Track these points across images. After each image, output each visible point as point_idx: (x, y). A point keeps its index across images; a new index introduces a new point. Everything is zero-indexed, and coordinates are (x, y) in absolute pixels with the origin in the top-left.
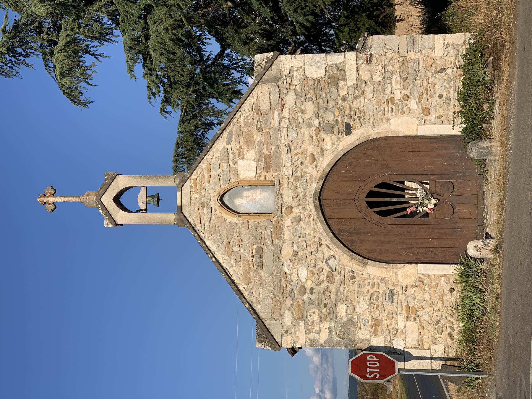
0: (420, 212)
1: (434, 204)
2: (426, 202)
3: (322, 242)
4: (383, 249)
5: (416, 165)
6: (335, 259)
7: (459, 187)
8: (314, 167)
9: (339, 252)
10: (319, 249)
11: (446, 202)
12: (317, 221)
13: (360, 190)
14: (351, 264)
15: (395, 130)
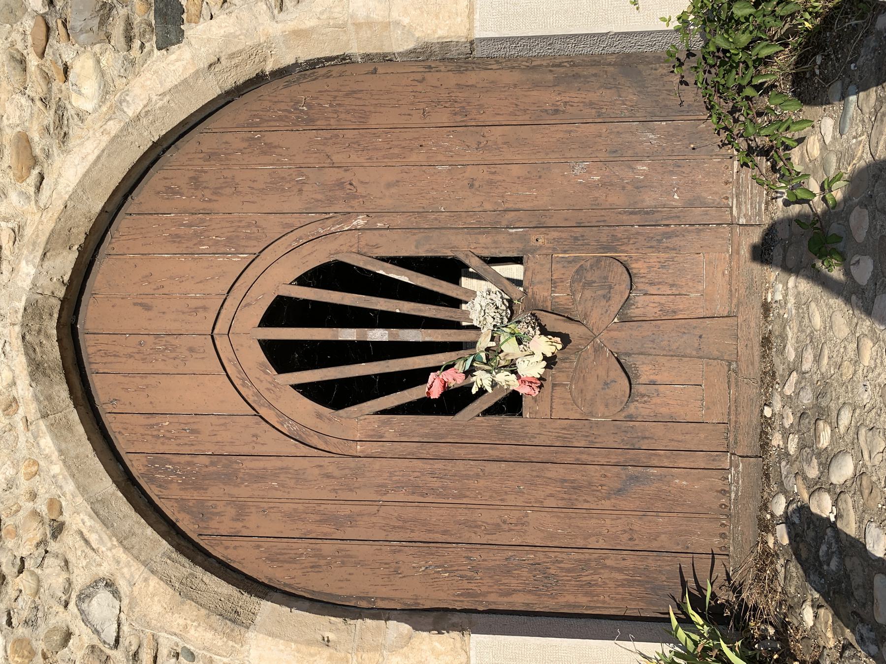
0: (482, 391)
1: (545, 358)
2: (510, 347)
3: (66, 517)
4: (328, 548)
5: (471, 186)
6: (116, 593)
7: (651, 284)
8: (32, 190)
9: (128, 565)
10: (53, 546)
11: (598, 350)
12: (38, 426)
13: (238, 293)
14: (177, 621)
15: (374, 16)
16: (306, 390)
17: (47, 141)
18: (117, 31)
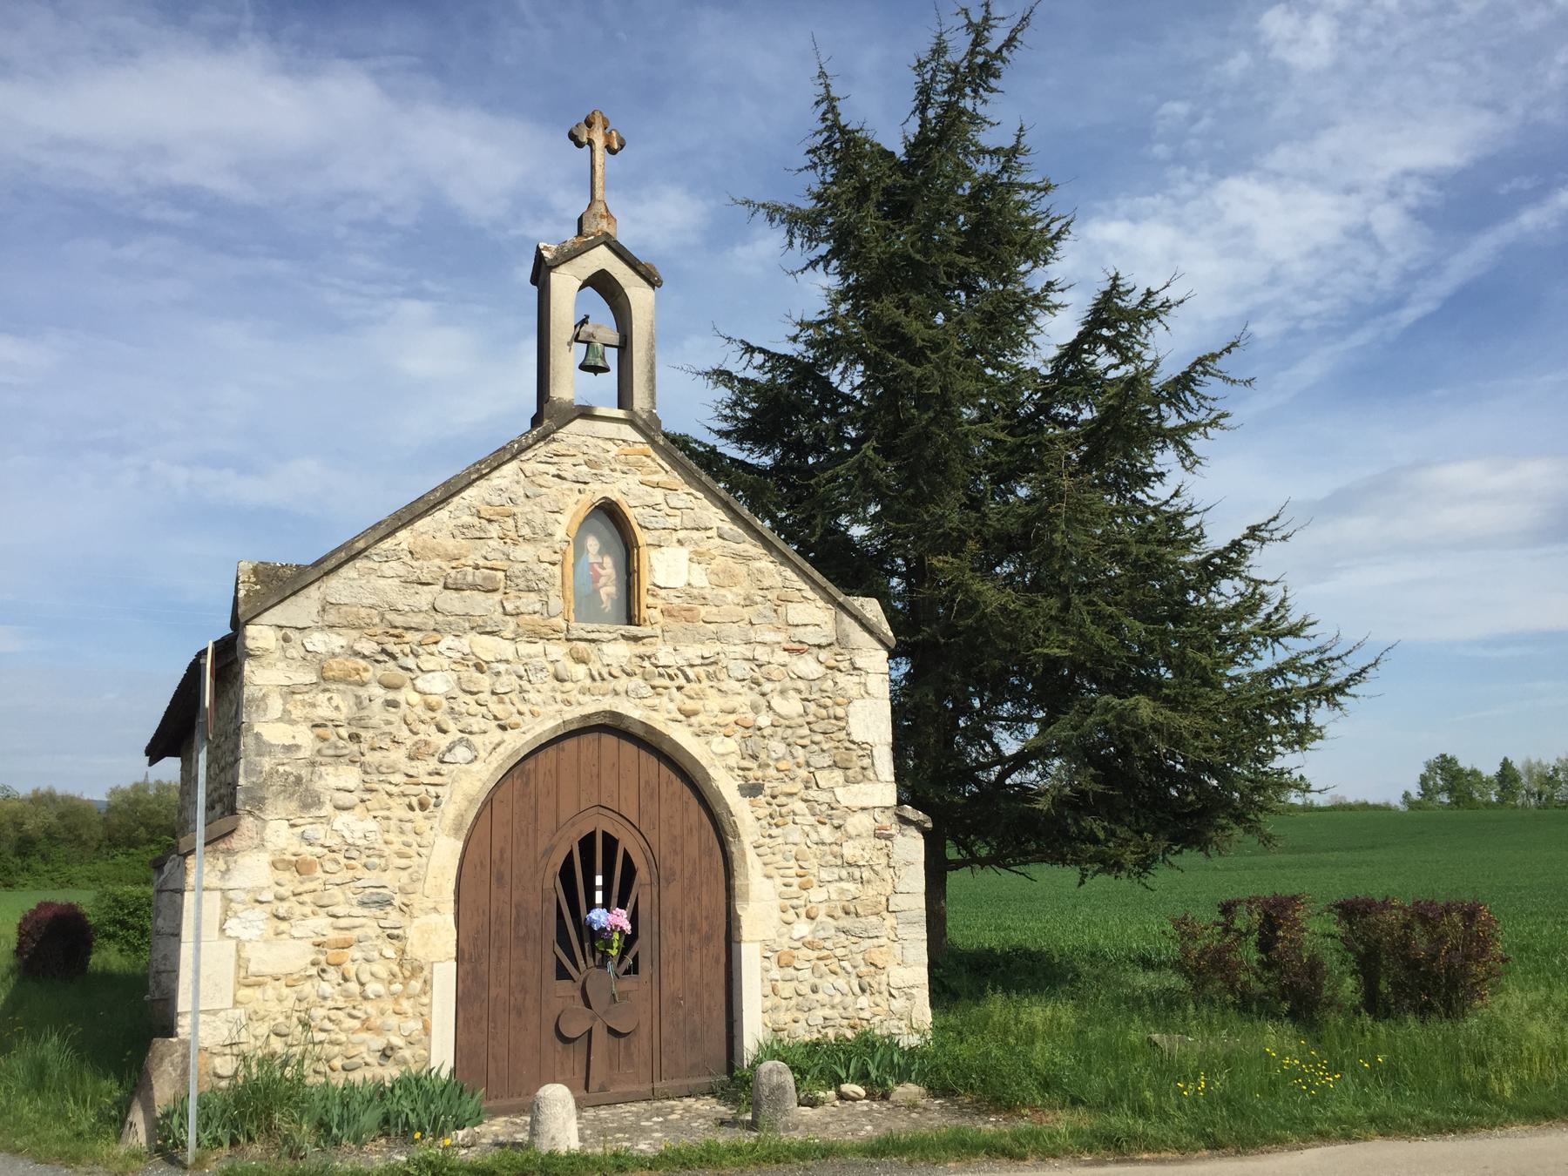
14: (458, 797)
16: (570, 856)
17: (696, 724)
18: (746, 764)
